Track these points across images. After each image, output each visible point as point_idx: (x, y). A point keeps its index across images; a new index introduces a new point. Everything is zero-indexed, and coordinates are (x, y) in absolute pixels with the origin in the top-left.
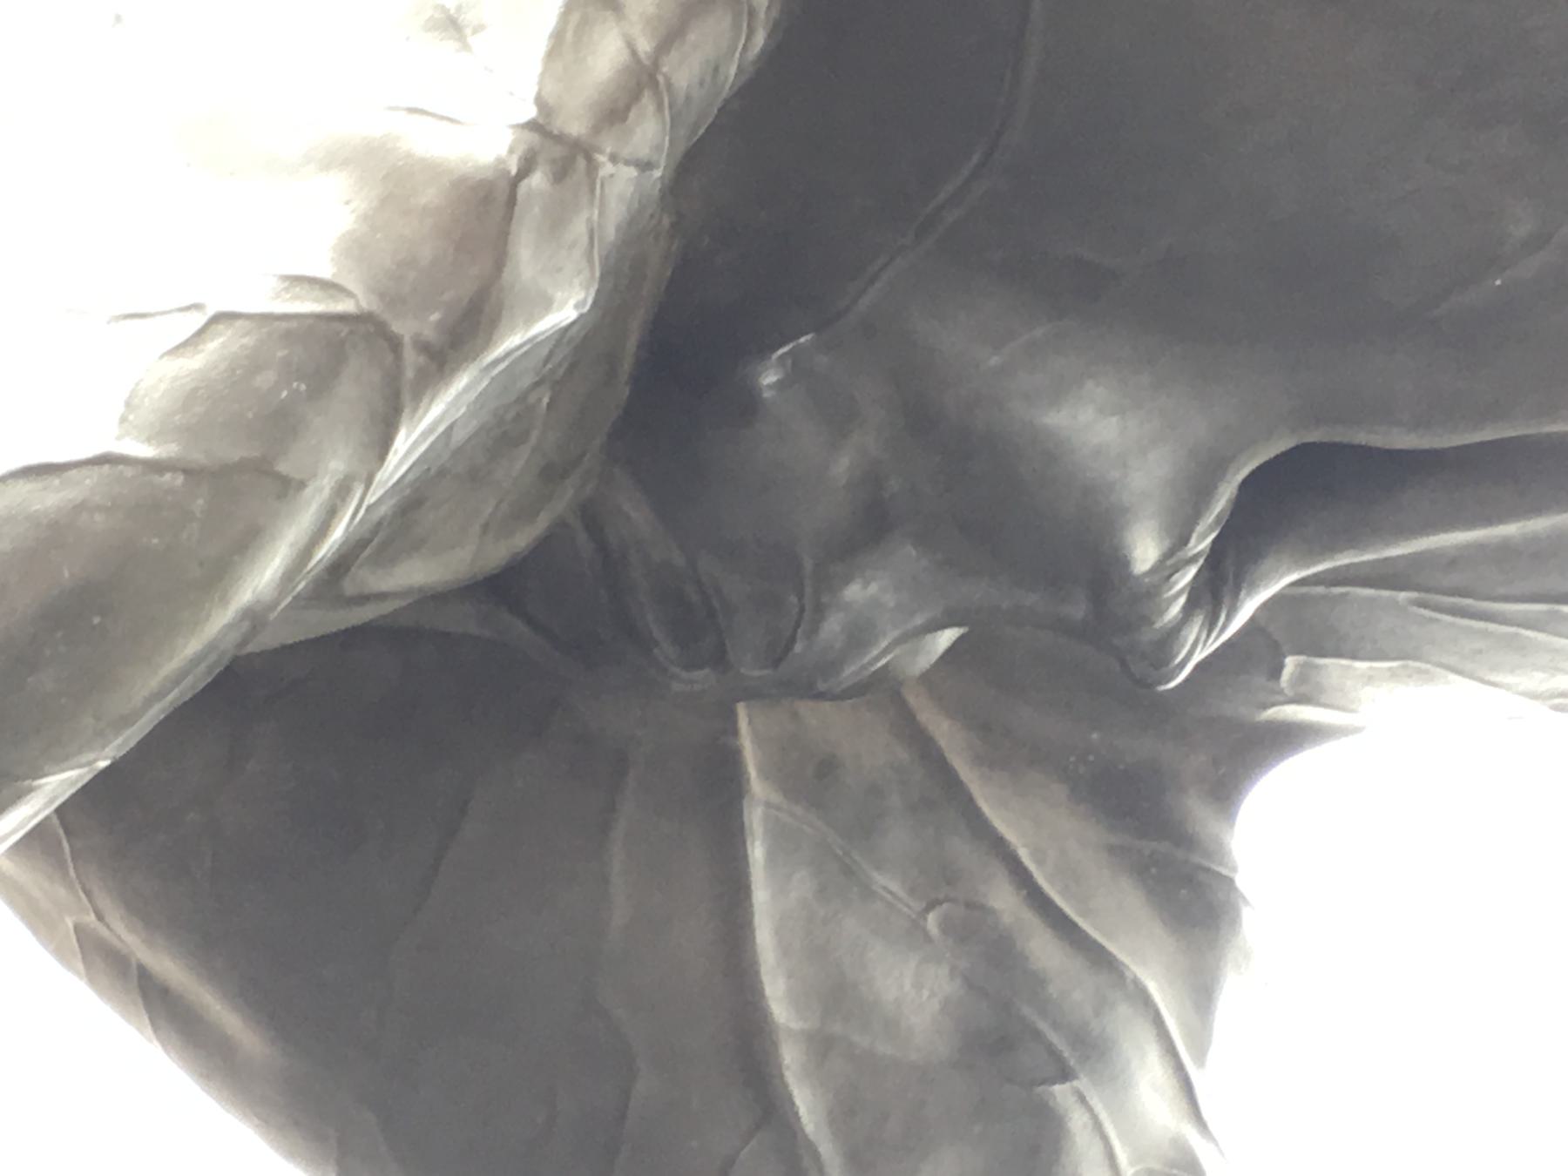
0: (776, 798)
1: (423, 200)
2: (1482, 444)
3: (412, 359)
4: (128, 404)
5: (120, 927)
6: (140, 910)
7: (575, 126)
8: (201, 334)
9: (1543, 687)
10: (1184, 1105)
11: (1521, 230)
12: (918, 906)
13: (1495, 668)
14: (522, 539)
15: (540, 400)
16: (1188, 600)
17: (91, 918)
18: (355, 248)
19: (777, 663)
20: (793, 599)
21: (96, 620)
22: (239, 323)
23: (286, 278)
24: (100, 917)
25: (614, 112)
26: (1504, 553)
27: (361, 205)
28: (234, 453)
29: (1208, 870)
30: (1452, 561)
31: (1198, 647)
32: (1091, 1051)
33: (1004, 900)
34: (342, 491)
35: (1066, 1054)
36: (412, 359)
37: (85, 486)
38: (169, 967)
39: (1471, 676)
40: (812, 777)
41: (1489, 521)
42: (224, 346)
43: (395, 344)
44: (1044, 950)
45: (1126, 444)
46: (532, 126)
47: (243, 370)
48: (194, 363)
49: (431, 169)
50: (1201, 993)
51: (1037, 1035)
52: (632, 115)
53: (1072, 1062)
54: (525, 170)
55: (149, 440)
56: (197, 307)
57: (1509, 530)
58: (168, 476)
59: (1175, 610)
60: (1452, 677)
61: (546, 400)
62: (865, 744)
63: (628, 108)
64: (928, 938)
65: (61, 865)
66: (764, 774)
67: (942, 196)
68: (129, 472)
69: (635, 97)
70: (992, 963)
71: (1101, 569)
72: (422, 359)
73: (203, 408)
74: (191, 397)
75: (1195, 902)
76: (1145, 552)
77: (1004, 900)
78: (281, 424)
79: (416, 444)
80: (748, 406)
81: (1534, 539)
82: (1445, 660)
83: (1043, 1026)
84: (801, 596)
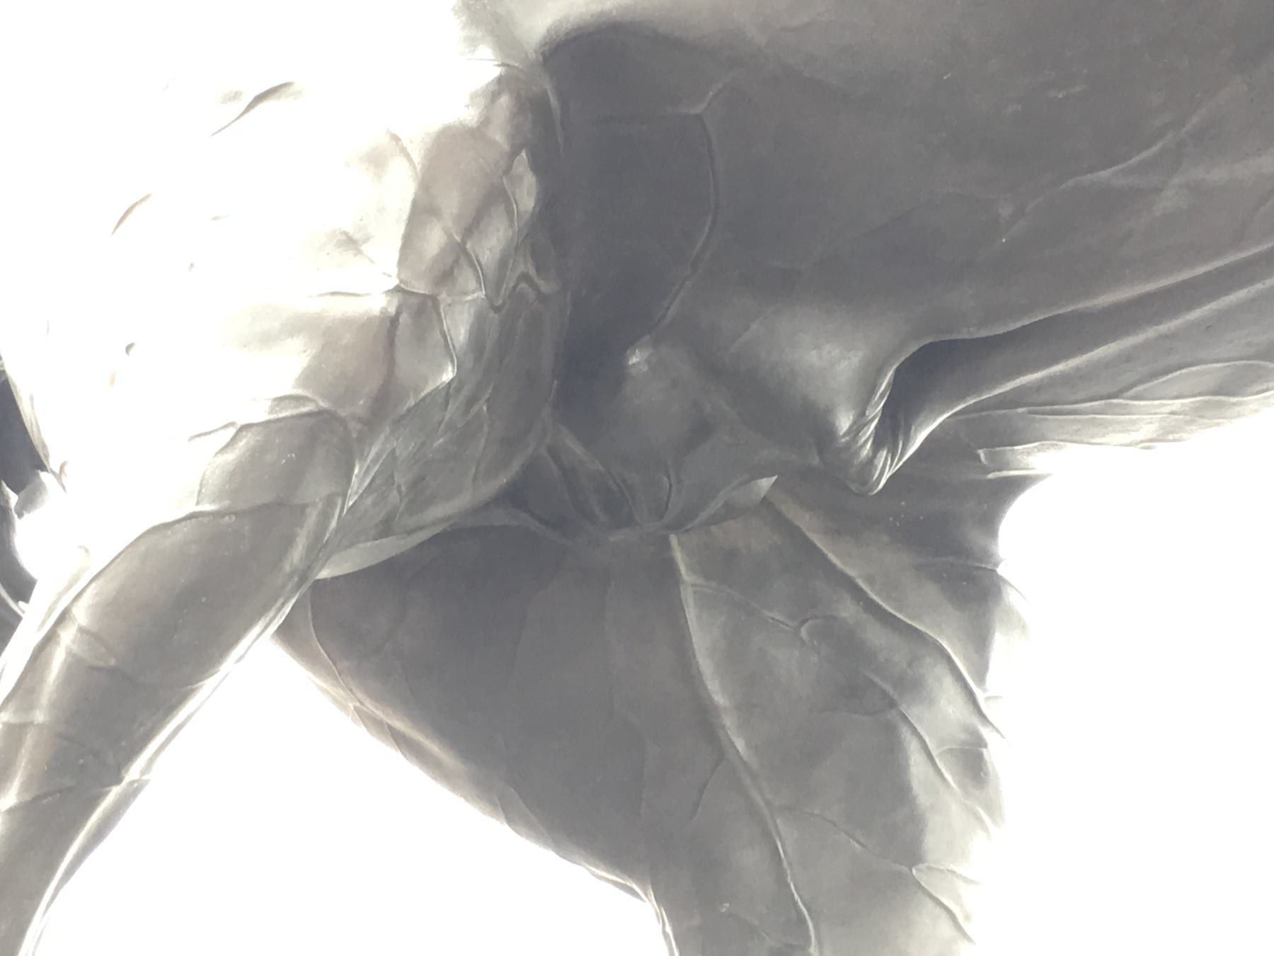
0: (701, 581)
1: (344, 342)
2: (1023, 327)
3: (354, 427)
4: (201, 485)
5: (369, 706)
6: (378, 699)
7: (421, 287)
8: (234, 440)
9: (1128, 441)
10: (971, 708)
11: (1005, 211)
12: (795, 624)
13: (1092, 436)
14: (516, 466)
15: (481, 409)
16: (874, 442)
17: (358, 704)
18: (309, 377)
19: (662, 517)
20: (666, 479)
21: (204, 600)
22: (254, 429)
23: (275, 399)
24: (361, 703)
25: (445, 276)
26: (1065, 380)
27: (312, 352)
28: (268, 498)
29: (978, 568)
30: (1040, 387)
31: (885, 469)
32: (912, 685)
33: (848, 611)
34: (330, 502)
35: (891, 692)
36: (354, 427)
37: (186, 527)
38: (400, 725)
39: (1081, 442)
40: (721, 565)
41: (1048, 364)
42: (248, 443)
43: (342, 421)
44: (876, 636)
45: (833, 362)
46: (397, 289)
47: (254, 457)
48: (231, 457)
49: (347, 322)
50: (980, 642)
51: (875, 685)
52: (456, 272)
53: (896, 697)
54: (398, 313)
55: (213, 501)
56: (232, 424)
57: (1164, 328)
58: (227, 518)
59: (866, 450)
60: (1069, 444)
61: (485, 408)
62: (754, 539)
63: (452, 269)
64: (803, 642)
65: (336, 679)
66: (691, 569)
67: (698, 246)
68: (205, 520)
69: (456, 262)
70: (845, 646)
71: (823, 433)
72: (359, 427)
73: (239, 478)
74: (232, 474)
75: (973, 588)
76: (844, 422)
77: (848, 611)
78: (294, 476)
79: (368, 469)
80: (620, 374)
81: (1078, 369)
82: (1064, 437)
83: (876, 679)
84: (669, 477)
